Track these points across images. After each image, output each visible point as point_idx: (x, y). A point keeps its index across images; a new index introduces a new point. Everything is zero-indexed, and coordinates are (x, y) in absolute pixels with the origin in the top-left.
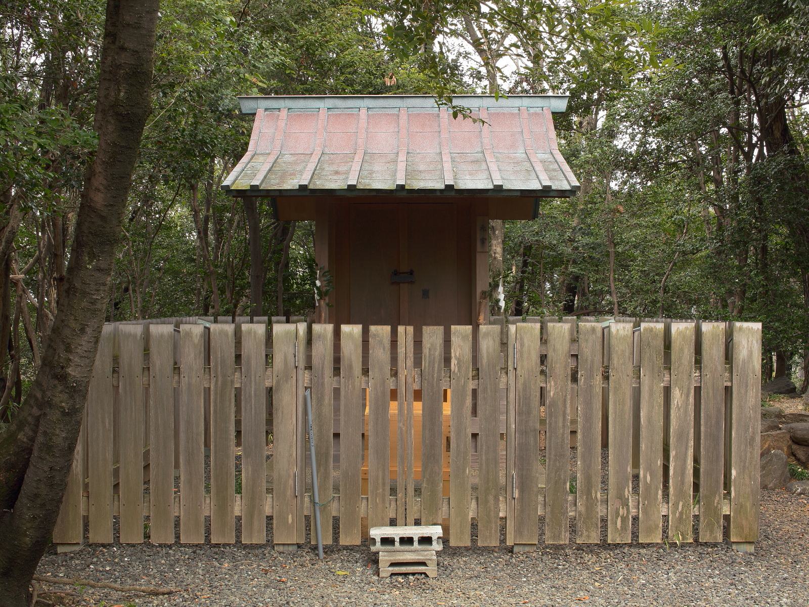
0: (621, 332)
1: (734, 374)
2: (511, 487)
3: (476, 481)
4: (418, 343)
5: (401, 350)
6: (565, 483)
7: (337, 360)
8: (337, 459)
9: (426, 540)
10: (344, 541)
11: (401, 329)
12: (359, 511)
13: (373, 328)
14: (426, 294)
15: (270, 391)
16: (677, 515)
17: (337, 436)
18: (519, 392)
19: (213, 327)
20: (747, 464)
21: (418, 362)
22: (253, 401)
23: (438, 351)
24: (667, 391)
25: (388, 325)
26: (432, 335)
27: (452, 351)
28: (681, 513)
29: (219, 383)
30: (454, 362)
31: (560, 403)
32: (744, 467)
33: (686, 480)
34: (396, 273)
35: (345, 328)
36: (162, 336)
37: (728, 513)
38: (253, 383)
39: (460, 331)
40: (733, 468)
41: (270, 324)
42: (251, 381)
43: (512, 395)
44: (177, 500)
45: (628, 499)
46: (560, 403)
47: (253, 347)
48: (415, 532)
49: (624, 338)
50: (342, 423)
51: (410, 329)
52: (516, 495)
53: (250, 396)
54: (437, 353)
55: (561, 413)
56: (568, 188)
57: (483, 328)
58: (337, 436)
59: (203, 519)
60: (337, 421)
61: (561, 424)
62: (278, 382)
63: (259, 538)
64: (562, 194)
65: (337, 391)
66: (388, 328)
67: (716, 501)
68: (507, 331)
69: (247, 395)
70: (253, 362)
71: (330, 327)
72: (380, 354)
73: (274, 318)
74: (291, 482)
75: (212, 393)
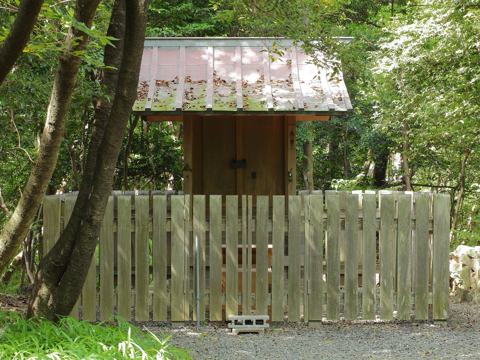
1: (434, 224)
2: (307, 289)
12: (221, 302)
13: (228, 197)
14: (254, 175)
16: (402, 304)
18: (311, 234)
20: (442, 275)
22: (160, 239)
23: (266, 209)
25: (218, 194)
26: (262, 201)
27: (273, 210)
28: (404, 303)
29: (141, 229)
32: (440, 276)
33: (407, 284)
34: (234, 161)
37: (431, 303)
38: (160, 230)
39: (278, 200)
40: (434, 277)
42: (158, 228)
44: (116, 296)
45: (374, 295)
51: (250, 197)
52: (310, 292)
53: (158, 237)
55: (336, 246)
57: (290, 197)
63: (163, 318)
66: (220, 197)
67: (424, 296)
68: (337, 258)
69: (156, 236)
70: (160, 217)
72: (232, 210)
73: (153, 192)
74: (181, 286)
75: (136, 235)
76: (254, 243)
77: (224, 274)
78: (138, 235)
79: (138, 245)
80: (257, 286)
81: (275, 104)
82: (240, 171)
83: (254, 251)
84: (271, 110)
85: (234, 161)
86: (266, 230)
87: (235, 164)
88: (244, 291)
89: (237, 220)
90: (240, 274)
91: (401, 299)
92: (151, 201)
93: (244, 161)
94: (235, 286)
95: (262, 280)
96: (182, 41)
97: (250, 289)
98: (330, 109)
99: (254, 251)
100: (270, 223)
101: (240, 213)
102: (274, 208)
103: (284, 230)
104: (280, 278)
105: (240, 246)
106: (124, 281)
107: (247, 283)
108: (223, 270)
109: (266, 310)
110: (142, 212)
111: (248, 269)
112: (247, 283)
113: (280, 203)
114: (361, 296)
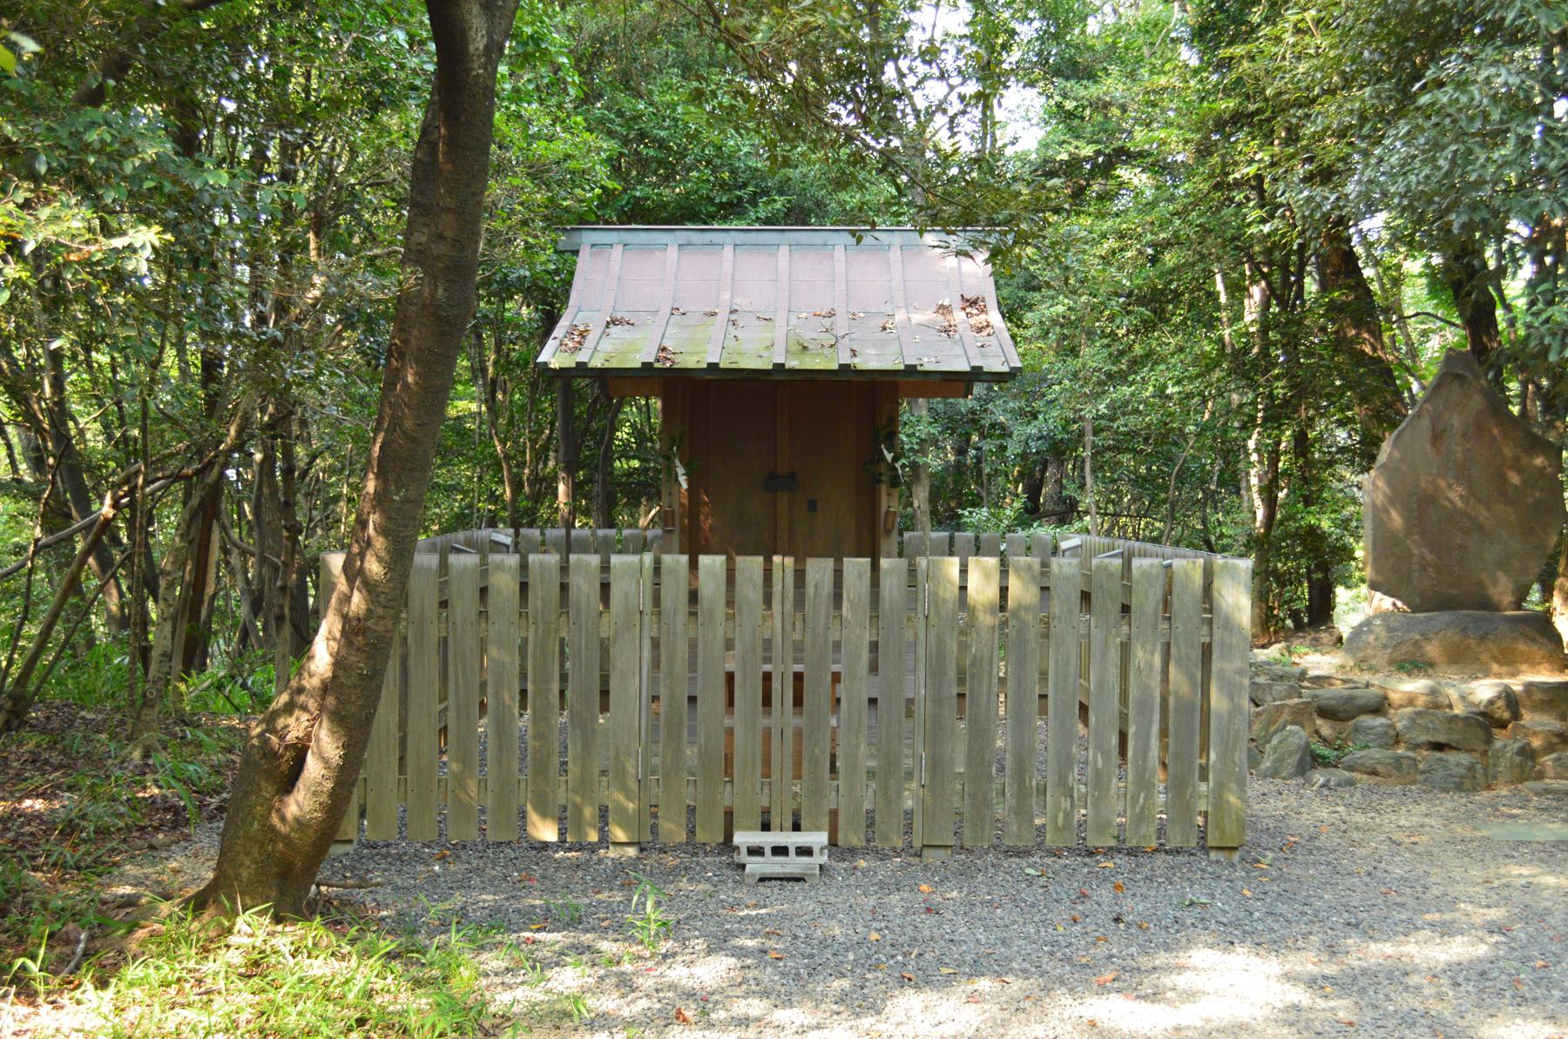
0: (1065, 570)
3: (872, 763)
4: (800, 575)
5: (777, 588)
6: (990, 766)
7: (694, 597)
8: (693, 731)
9: (805, 851)
10: (701, 836)
11: (777, 559)
14: (812, 506)
15: (604, 648)
17: (692, 700)
19: (1177, 563)
21: (800, 602)
24: (1126, 648)
25: (829, 556)
26: (819, 570)
28: (1142, 809)
30: (845, 605)
31: (986, 661)
34: (772, 476)
35: (704, 560)
36: (465, 569)
39: (855, 567)
41: (839, 561)
43: (921, 651)
46: (986, 661)
47: (584, 585)
48: (793, 839)
49: (1068, 578)
50: (700, 683)
51: (789, 561)
54: (825, 593)
56: (1005, 369)
57: (884, 563)
58: (692, 700)
59: (515, 810)
60: (693, 680)
61: (985, 689)
62: (616, 632)
64: (998, 377)
65: (693, 645)
71: (684, 559)
72: (750, 591)
76: (796, 661)
77: (730, 732)
78: (535, 645)
79: (534, 668)
80: (805, 765)
81: (854, 353)
82: (783, 498)
83: (798, 677)
84: (845, 368)
85: (772, 476)
86: (826, 639)
87: (775, 482)
88: (775, 776)
89: (759, 610)
90: (767, 734)
91: (1135, 799)
92: (564, 569)
93: (793, 476)
94: (754, 765)
95: (817, 750)
96: (672, 234)
97: (789, 773)
98: (973, 368)
99: (798, 677)
100: (837, 622)
101: (768, 600)
102: (845, 574)
103: (867, 637)
104: (858, 747)
105: (767, 668)
106: (500, 749)
107: (782, 754)
108: (727, 722)
109: (826, 820)
110: (544, 593)
111: (783, 716)
112: (782, 754)
113: (860, 576)
114: (1042, 791)
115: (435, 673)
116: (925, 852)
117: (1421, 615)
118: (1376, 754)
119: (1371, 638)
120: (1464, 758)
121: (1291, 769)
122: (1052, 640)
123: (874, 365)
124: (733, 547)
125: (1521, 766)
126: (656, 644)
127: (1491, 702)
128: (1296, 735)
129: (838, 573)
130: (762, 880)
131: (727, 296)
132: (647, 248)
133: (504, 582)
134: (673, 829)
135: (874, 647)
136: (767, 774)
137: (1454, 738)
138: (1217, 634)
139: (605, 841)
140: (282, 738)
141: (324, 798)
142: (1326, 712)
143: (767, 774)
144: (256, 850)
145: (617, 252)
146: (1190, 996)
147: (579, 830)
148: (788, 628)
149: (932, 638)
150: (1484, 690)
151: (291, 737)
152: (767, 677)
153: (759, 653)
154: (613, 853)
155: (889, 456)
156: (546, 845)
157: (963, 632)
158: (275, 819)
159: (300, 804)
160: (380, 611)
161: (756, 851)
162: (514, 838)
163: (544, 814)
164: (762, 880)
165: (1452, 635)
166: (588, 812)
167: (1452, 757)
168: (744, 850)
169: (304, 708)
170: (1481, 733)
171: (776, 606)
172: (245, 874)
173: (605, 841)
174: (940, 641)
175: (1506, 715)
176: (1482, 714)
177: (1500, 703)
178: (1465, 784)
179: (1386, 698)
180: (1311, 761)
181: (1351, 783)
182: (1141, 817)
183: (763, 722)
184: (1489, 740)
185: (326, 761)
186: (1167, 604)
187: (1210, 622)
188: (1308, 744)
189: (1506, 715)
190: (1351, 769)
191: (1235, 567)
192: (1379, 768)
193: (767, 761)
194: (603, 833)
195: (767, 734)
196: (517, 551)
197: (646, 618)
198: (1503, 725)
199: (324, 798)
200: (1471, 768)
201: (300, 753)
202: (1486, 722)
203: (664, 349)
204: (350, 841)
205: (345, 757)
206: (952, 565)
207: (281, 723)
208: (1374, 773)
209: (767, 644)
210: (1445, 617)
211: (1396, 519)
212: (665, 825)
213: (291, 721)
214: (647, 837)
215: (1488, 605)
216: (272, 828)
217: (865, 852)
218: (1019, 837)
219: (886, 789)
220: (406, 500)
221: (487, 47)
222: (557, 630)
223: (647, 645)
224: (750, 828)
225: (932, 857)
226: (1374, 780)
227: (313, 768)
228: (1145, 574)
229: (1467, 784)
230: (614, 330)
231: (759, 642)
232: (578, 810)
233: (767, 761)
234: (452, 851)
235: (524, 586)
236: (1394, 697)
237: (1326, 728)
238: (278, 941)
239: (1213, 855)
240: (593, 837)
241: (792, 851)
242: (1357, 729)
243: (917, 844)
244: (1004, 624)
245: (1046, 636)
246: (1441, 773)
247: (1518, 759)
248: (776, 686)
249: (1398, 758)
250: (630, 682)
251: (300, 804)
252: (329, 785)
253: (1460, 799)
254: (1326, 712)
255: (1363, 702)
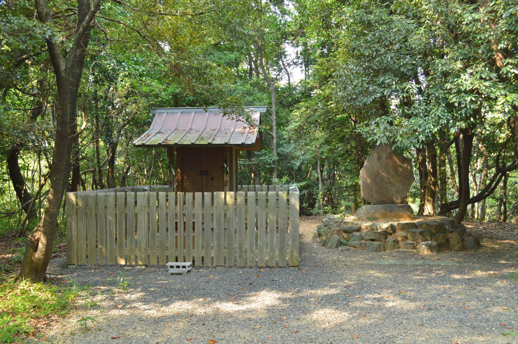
14: (212, 179)
47: (131, 200)
87: (203, 173)
90: (176, 237)
97: (182, 247)
101: (176, 204)
105: (176, 221)
109: (192, 260)
110: (121, 202)
114: (246, 252)
115: (95, 223)
116: (217, 267)
117: (375, 206)
118: (356, 242)
119: (362, 212)
120: (378, 243)
121: (335, 246)
122: (248, 213)
123: (218, 143)
124: (194, 190)
125: (394, 245)
126: (148, 214)
127: (387, 228)
128: (336, 237)
129: (194, 196)
130: (172, 274)
131: (190, 126)
132: (173, 113)
133: (111, 200)
134: (153, 261)
135: (203, 215)
136: (177, 247)
137: (376, 238)
138: (290, 211)
139: (137, 265)
140: (34, 238)
141: (43, 253)
142: (345, 231)
143: (177, 247)
144: (29, 265)
145: (165, 114)
146: (250, 302)
147: (130, 262)
148: (181, 210)
149: (218, 213)
150: (385, 226)
151: (36, 238)
152: (176, 223)
153: (174, 216)
154: (138, 267)
155: (226, 166)
156: (122, 266)
157: (225, 211)
158: (33, 258)
159: (38, 255)
160: (52, 207)
161: (172, 267)
162: (115, 264)
163: (121, 257)
164: (172, 274)
165: (383, 211)
166: (133, 257)
167: (375, 243)
168: (169, 267)
169: (40, 231)
170: (384, 236)
171: (178, 204)
172: (26, 272)
173: (137, 265)
174: (219, 213)
175: (391, 232)
176: (385, 231)
177: (390, 228)
178: (378, 249)
179: (361, 227)
180: (340, 244)
181: (349, 250)
182: (272, 258)
183: (176, 234)
184: (386, 239)
185: (43, 243)
186: (126, 203)
187: (289, 208)
188: (339, 240)
189: (391, 232)
190: (349, 246)
191: (295, 194)
192: (356, 246)
193: (177, 245)
194: (136, 262)
195: (176, 237)
196: (255, 191)
197: (146, 208)
198: (391, 234)
199: (43, 253)
200: (380, 245)
201: (38, 240)
202: (386, 234)
203: (166, 140)
204: (74, 264)
205: (47, 242)
206: (222, 194)
207: (34, 234)
208: (355, 247)
209: (176, 215)
210: (381, 206)
211: (369, 180)
212: (151, 261)
213: (37, 234)
214: (147, 264)
215: (394, 203)
216: (33, 260)
217: (201, 267)
218: (240, 263)
219: (207, 251)
220: (57, 179)
221: (65, 69)
222: (125, 211)
223: (146, 214)
224: (172, 261)
225: (219, 269)
226: (355, 249)
227: (40, 245)
228: (272, 195)
229: (378, 250)
230: (158, 135)
231: (174, 214)
232: (130, 257)
233: (177, 245)
234: (98, 266)
235: (246, 200)
236: (363, 227)
237: (345, 235)
238: (31, 288)
239: (291, 268)
240: (134, 263)
241: (181, 267)
242: (353, 236)
243: (215, 265)
244: (236, 209)
245: (247, 212)
246: (371, 247)
247: (393, 243)
248: (179, 225)
249: (361, 243)
250: (143, 225)
251: (38, 255)
252: (44, 249)
253: (375, 254)
254: (345, 231)
255: (354, 228)
